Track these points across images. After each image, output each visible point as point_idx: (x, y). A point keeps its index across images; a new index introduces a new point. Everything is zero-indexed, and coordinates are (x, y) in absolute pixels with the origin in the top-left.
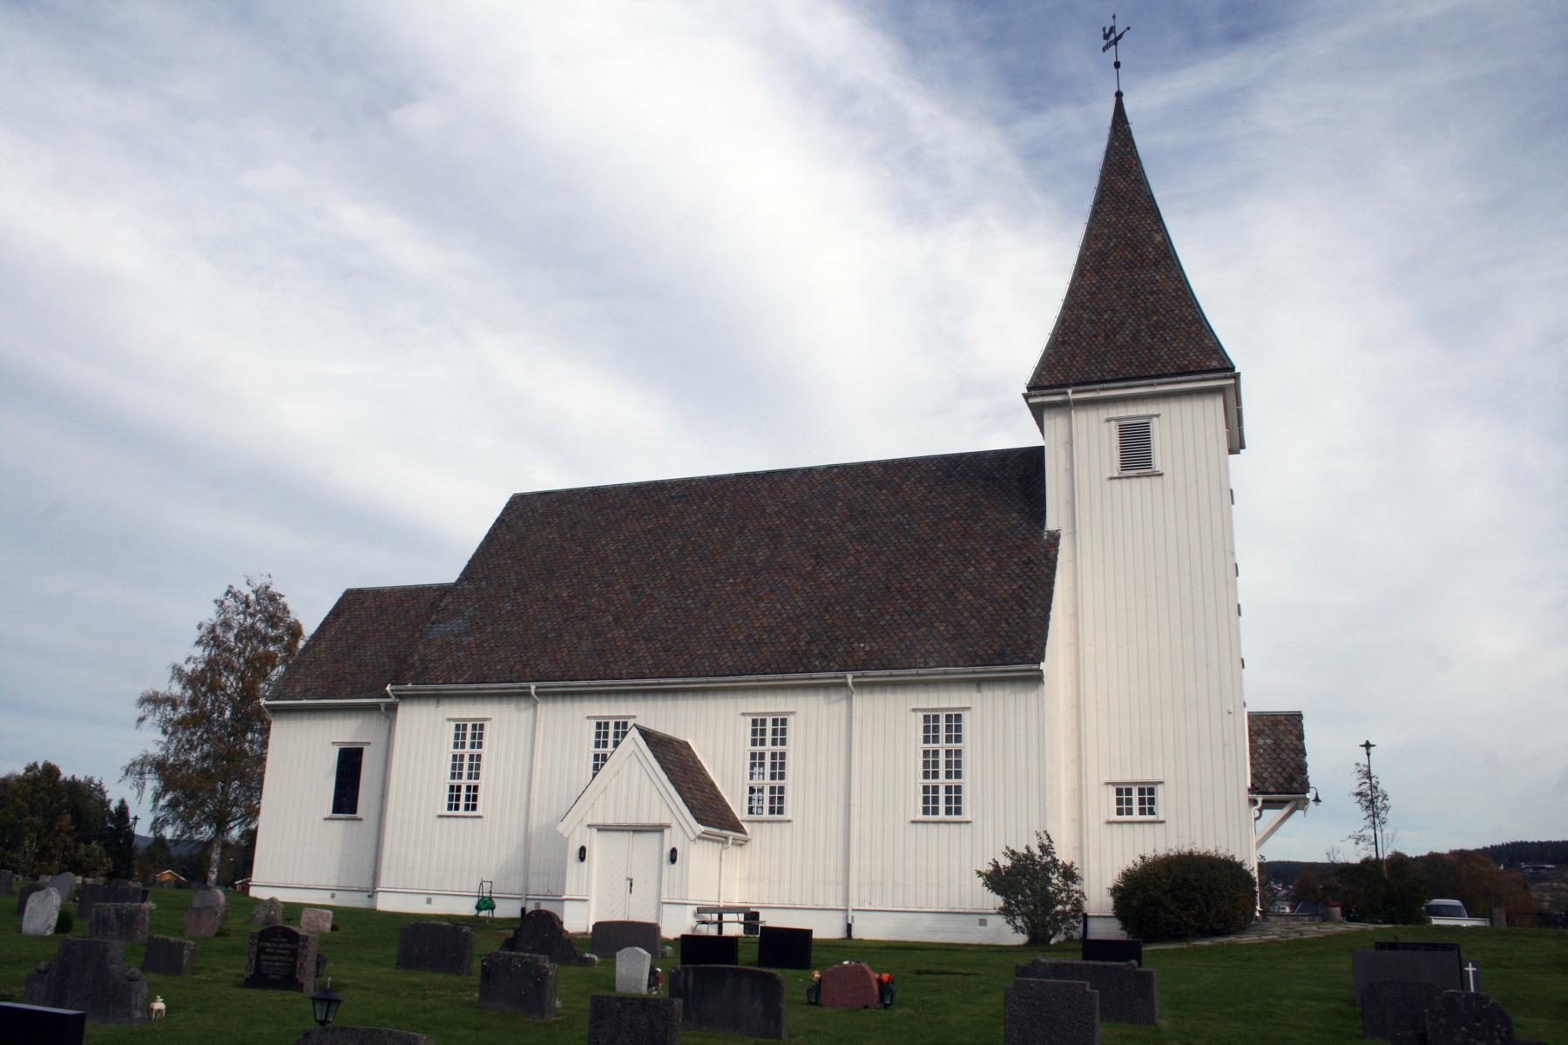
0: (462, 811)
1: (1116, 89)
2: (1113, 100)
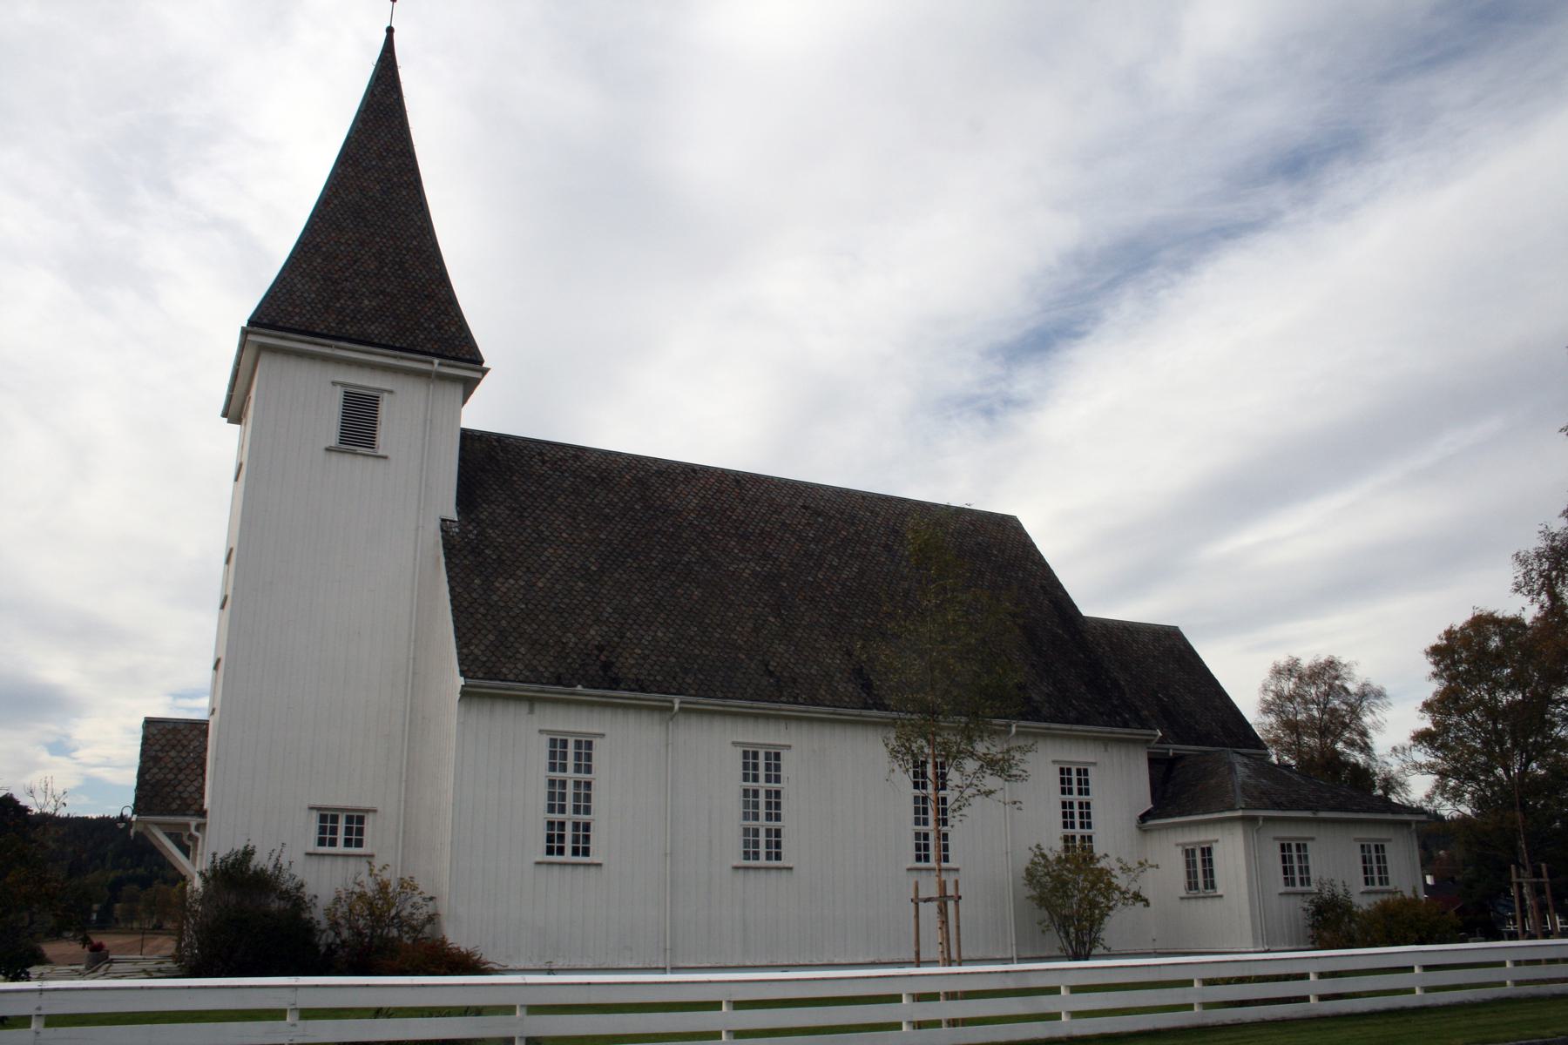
0: (568, 856)
1: (389, 25)
2: (384, 35)
